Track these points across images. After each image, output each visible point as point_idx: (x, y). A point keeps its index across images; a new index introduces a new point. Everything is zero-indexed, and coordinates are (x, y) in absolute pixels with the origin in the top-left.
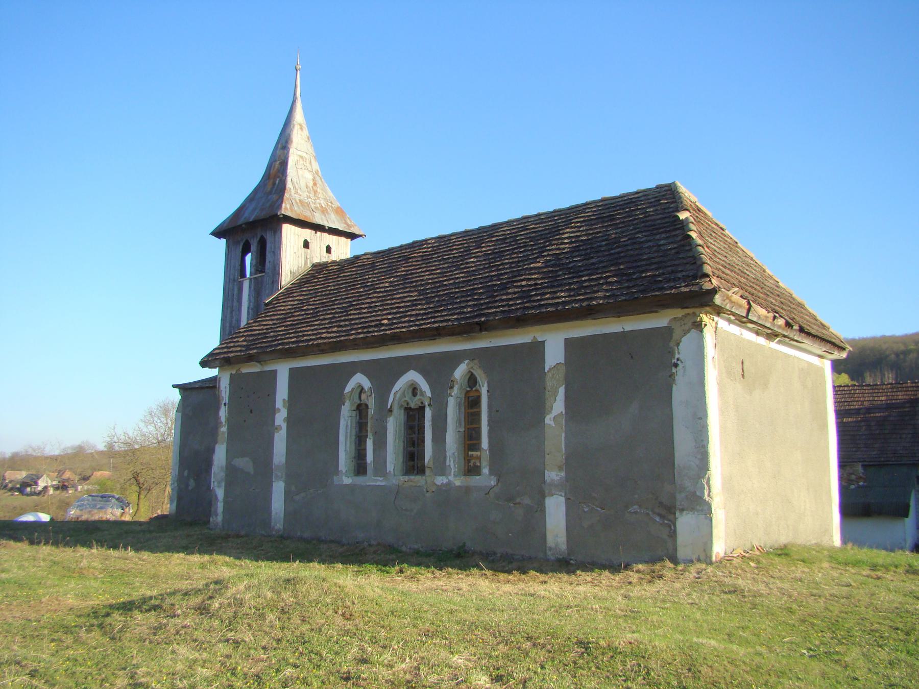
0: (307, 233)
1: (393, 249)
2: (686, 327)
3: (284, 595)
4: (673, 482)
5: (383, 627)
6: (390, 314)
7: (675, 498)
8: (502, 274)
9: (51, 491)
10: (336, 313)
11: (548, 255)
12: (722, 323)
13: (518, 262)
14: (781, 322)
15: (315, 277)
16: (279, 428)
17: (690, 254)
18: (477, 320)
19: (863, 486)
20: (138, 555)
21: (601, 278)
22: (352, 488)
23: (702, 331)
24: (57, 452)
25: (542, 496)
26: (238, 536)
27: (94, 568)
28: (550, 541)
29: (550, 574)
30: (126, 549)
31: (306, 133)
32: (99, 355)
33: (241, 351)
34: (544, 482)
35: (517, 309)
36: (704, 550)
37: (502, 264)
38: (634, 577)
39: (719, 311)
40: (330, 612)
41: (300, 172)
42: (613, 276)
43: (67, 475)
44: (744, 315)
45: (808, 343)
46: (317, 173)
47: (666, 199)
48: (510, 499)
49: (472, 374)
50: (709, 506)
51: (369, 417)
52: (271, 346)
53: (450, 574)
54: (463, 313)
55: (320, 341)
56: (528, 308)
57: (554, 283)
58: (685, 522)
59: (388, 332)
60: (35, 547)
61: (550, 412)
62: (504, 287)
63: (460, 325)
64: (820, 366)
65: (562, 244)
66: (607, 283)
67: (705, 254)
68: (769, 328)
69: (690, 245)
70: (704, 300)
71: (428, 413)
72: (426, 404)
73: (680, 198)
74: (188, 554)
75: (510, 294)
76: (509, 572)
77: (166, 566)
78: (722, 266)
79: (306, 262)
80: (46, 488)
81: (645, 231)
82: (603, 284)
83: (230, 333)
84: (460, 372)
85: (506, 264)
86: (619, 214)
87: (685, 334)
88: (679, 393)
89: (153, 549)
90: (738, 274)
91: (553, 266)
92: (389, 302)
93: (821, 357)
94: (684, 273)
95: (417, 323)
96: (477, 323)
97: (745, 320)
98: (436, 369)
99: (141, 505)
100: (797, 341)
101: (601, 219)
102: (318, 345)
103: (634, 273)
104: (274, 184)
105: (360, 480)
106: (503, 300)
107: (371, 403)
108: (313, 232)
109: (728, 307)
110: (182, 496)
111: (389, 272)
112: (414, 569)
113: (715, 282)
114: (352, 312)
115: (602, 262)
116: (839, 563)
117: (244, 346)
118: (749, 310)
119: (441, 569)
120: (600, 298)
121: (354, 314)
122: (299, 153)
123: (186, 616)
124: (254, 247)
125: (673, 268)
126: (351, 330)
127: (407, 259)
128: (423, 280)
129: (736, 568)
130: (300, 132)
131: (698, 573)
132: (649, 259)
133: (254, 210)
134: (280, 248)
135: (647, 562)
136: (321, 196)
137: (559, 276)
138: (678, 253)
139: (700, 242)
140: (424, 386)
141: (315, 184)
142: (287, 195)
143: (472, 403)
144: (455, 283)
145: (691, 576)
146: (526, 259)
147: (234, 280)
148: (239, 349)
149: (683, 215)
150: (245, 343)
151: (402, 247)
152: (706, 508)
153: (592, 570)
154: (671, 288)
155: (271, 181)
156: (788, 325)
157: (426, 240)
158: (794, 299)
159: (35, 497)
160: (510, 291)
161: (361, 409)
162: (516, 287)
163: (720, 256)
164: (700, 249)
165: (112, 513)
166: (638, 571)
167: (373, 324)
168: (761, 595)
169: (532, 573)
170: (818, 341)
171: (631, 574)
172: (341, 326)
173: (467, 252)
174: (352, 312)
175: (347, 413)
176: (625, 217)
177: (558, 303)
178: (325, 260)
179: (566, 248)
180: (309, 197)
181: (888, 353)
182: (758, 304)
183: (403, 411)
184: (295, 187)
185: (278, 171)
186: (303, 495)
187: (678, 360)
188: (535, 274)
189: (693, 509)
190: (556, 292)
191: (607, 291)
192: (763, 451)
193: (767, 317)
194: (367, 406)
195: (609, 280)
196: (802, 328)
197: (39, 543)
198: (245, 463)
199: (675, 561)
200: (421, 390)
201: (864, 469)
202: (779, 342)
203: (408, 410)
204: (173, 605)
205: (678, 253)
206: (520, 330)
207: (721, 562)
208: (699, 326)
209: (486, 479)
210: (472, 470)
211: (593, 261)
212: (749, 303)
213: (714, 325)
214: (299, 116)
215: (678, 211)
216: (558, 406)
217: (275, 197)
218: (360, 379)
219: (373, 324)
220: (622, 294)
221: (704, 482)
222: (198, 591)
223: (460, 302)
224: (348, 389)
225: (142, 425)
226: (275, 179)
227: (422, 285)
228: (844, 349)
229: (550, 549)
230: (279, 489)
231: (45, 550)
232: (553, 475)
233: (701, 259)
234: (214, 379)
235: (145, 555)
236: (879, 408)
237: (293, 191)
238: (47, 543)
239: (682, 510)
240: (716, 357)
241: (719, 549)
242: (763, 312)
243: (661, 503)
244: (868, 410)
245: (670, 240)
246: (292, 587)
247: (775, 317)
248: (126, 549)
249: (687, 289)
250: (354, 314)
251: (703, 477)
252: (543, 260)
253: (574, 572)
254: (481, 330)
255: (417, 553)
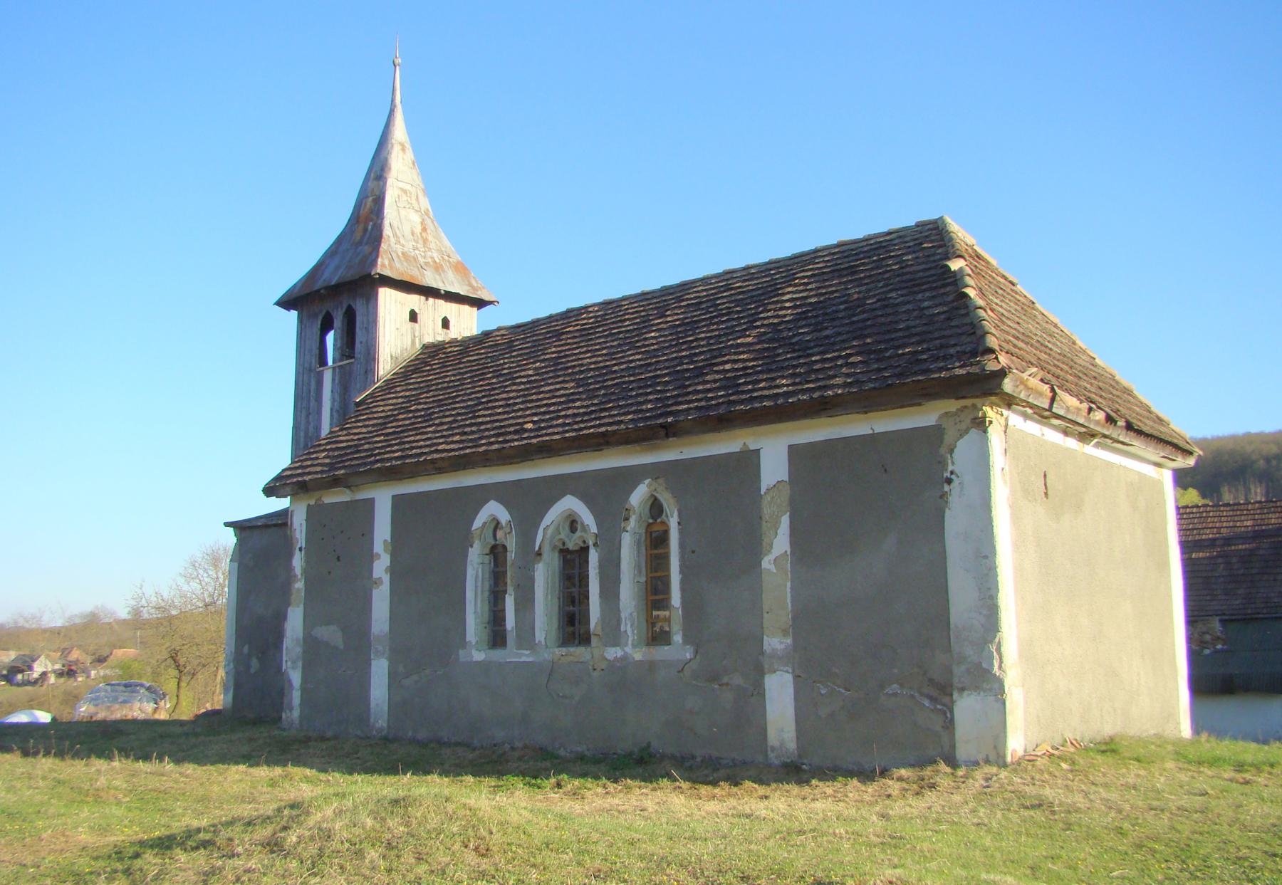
0: (414, 301)
1: (538, 320)
2: (963, 426)
3: (390, 823)
4: (948, 649)
5: (534, 866)
6: (535, 414)
7: (951, 672)
8: (696, 355)
9: (52, 679)
10: (459, 414)
11: (763, 325)
12: (1015, 419)
13: (719, 336)
14: (1099, 416)
15: (427, 364)
16: (379, 582)
17: (967, 320)
18: (661, 421)
19: (1222, 650)
20: (178, 769)
21: (839, 357)
22: (485, 666)
23: (985, 431)
24: (59, 623)
25: (758, 673)
26: (323, 739)
27: (116, 789)
28: (773, 737)
29: (774, 786)
30: (162, 760)
31: (410, 155)
32: (124, 486)
33: (322, 472)
34: (762, 653)
35: (719, 404)
36: (995, 747)
37: (696, 340)
38: (894, 787)
39: (1009, 402)
40: (457, 846)
41: (403, 212)
42: (857, 354)
43: (75, 654)
44: (1046, 406)
45: (1138, 446)
46: (427, 213)
47: (931, 241)
48: (714, 678)
49: (656, 499)
50: (1000, 683)
51: (509, 563)
52: (366, 464)
53: (629, 788)
54: (641, 411)
55: (435, 456)
56: (734, 402)
57: (772, 365)
58: (966, 707)
59: (534, 441)
60: (30, 759)
61: (770, 551)
62: (699, 372)
63: (637, 429)
64: (1155, 479)
65: (782, 309)
66: (847, 364)
67: (988, 320)
68: (1082, 425)
69: (967, 307)
70: (988, 385)
71: (593, 557)
72: (591, 543)
73: (951, 239)
74: (251, 766)
75: (707, 382)
76: (714, 783)
77: (219, 783)
78: (1014, 336)
79: (413, 343)
80: (44, 674)
81: (901, 289)
82: (841, 366)
83: (306, 447)
84: (639, 496)
85: (703, 339)
86: (863, 264)
87: (961, 436)
88: (955, 520)
89: (201, 760)
90: (1036, 349)
91: (770, 341)
92: (534, 397)
93: (1157, 465)
94: (958, 348)
95: (575, 427)
96: (662, 426)
97: (1047, 413)
98: (606, 492)
99: (182, 697)
100: (1123, 443)
101: (837, 272)
102: (433, 461)
103: (886, 349)
104: (365, 230)
105: (498, 655)
106: (698, 392)
107: (511, 544)
108: (423, 298)
109: (1022, 396)
110: (240, 682)
111: (533, 355)
112: (577, 782)
113: (1003, 360)
114: (481, 413)
115: (840, 334)
116: (1190, 762)
117: (326, 465)
118: (1053, 400)
119: (616, 781)
120: (838, 386)
121: (484, 416)
122: (401, 185)
123: (250, 855)
124: (338, 322)
125: (943, 341)
126: (481, 438)
127: (559, 334)
128: (582, 365)
129: (1041, 772)
130: (401, 154)
131: (987, 780)
132: (908, 328)
133: (337, 268)
134: (375, 322)
135: (912, 766)
136: (432, 246)
137: (778, 355)
138: (949, 319)
139: (980, 302)
140: (587, 517)
141: (424, 229)
142: (384, 246)
143: (656, 541)
144: (628, 368)
145: (977, 785)
146: (730, 332)
147: (310, 370)
148: (319, 469)
149: (955, 265)
150: (327, 461)
151: (551, 318)
152: (996, 686)
153: (834, 779)
154: (940, 370)
155: (361, 226)
156: (1110, 420)
157: (586, 308)
158: (1117, 383)
159: (29, 688)
160: (708, 378)
161: (497, 553)
162: (717, 372)
163: (1009, 323)
164: (981, 313)
165: (141, 709)
166: (900, 779)
167: (512, 429)
168: (1078, 810)
169: (748, 784)
170: (1153, 443)
171: (890, 783)
172: (465, 433)
173: (645, 324)
174: (481, 413)
175: (476, 558)
176: (872, 269)
177: (777, 394)
178: (440, 339)
179: (788, 314)
180: (416, 248)
181: (1254, 457)
182: (1066, 390)
183: (557, 554)
184: (395, 235)
185: (371, 211)
186: (415, 677)
187: (952, 473)
188: (743, 353)
189: (977, 688)
190: (774, 379)
191: (848, 375)
192: (1076, 601)
193: (1079, 409)
194: (504, 547)
195: (851, 360)
196: (1132, 425)
197: (36, 754)
198: (330, 634)
199: (953, 763)
200: (582, 524)
201: (1224, 626)
202: (1097, 445)
203: (564, 552)
204: (231, 840)
205: (949, 319)
206: (723, 435)
207: (1019, 764)
208: (981, 424)
209: (678, 649)
210: (658, 637)
211: (827, 332)
212: (1053, 390)
213: (1002, 421)
214: (400, 132)
215: (949, 259)
216: (780, 543)
217: (366, 249)
218: (494, 509)
219: (512, 429)
220: (870, 380)
221: (993, 648)
222: (267, 819)
223: (637, 396)
224: (478, 523)
225: (181, 581)
226: (366, 223)
227: (581, 372)
228: (1190, 453)
229: (773, 749)
230: (380, 670)
231: (46, 764)
232: (775, 643)
233: (982, 327)
234: (284, 513)
235: (190, 768)
236: (1242, 538)
237: (393, 240)
238: (47, 754)
239: (962, 690)
240: (1007, 468)
241: (1016, 744)
242: (1072, 402)
243: (931, 680)
244: (1228, 541)
245: (937, 301)
246: (401, 811)
247: (1090, 410)
248: (162, 760)
249: (962, 372)
250: (484, 416)
251: (991, 642)
252: (754, 332)
253: (807, 782)
254: (667, 436)
255: (582, 758)
